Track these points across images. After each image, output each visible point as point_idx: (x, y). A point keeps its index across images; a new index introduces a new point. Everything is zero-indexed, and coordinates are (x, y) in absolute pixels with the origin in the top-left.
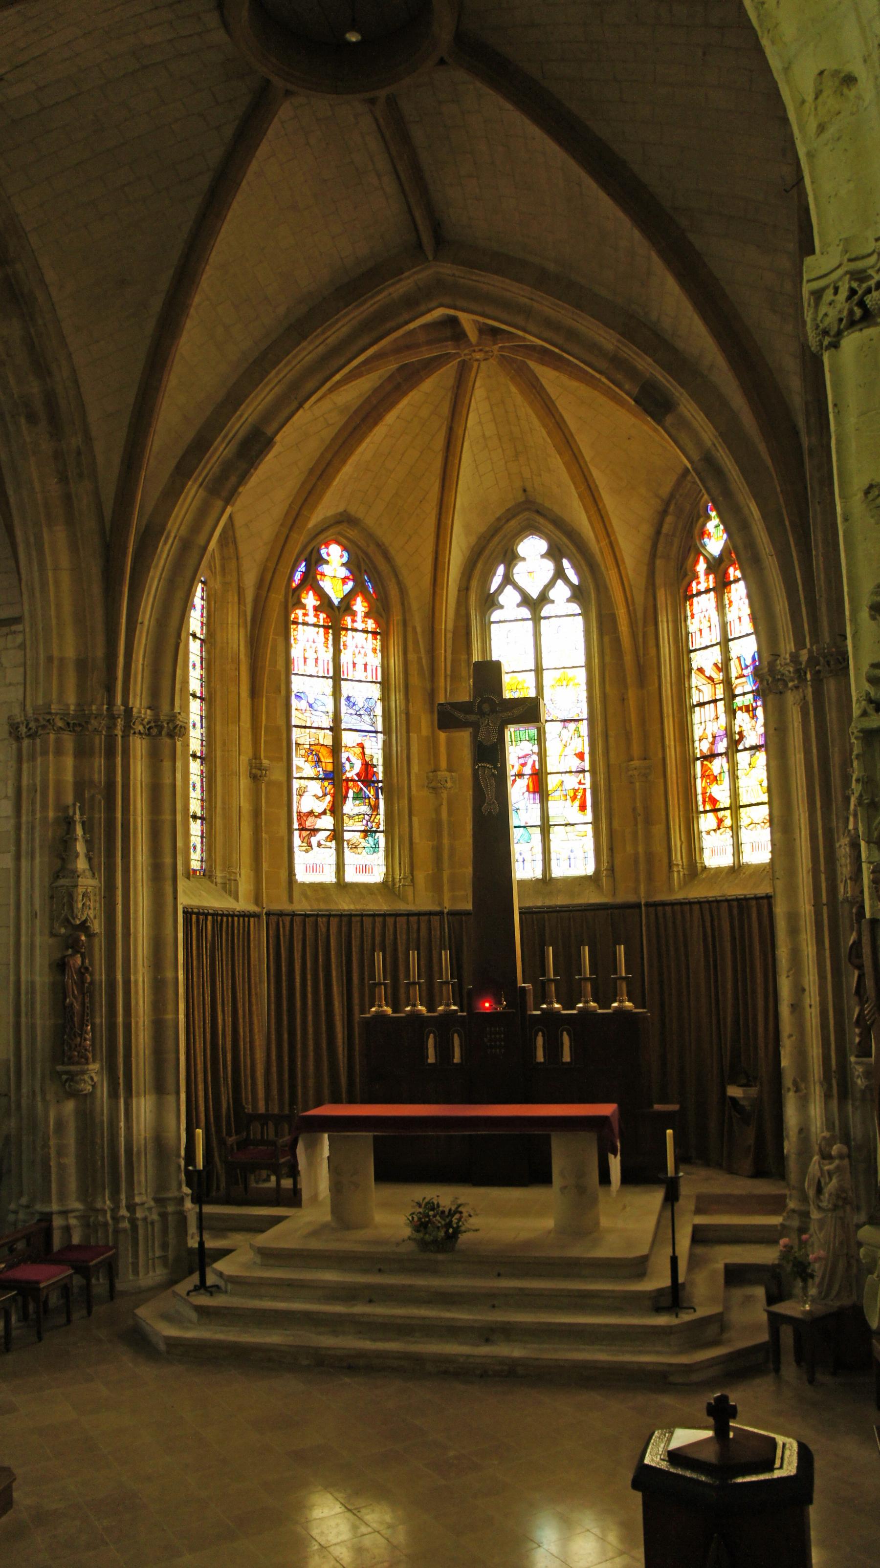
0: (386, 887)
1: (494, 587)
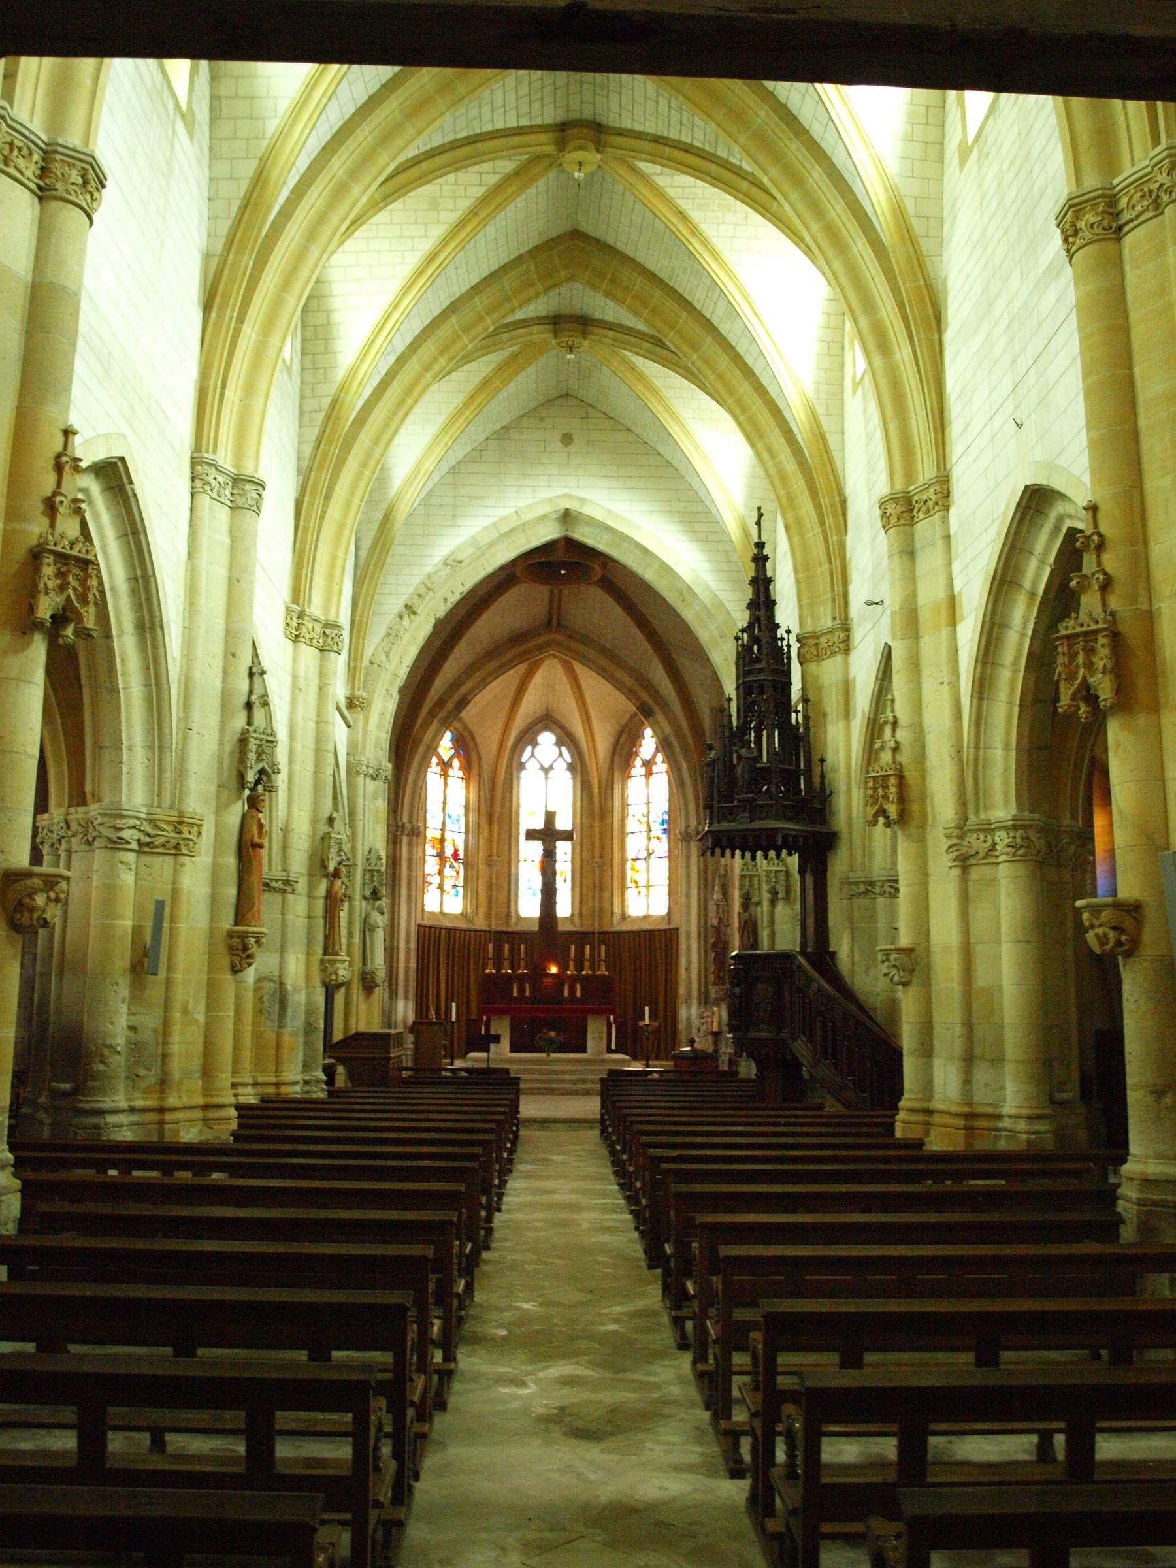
0: (464, 915)
1: (524, 759)
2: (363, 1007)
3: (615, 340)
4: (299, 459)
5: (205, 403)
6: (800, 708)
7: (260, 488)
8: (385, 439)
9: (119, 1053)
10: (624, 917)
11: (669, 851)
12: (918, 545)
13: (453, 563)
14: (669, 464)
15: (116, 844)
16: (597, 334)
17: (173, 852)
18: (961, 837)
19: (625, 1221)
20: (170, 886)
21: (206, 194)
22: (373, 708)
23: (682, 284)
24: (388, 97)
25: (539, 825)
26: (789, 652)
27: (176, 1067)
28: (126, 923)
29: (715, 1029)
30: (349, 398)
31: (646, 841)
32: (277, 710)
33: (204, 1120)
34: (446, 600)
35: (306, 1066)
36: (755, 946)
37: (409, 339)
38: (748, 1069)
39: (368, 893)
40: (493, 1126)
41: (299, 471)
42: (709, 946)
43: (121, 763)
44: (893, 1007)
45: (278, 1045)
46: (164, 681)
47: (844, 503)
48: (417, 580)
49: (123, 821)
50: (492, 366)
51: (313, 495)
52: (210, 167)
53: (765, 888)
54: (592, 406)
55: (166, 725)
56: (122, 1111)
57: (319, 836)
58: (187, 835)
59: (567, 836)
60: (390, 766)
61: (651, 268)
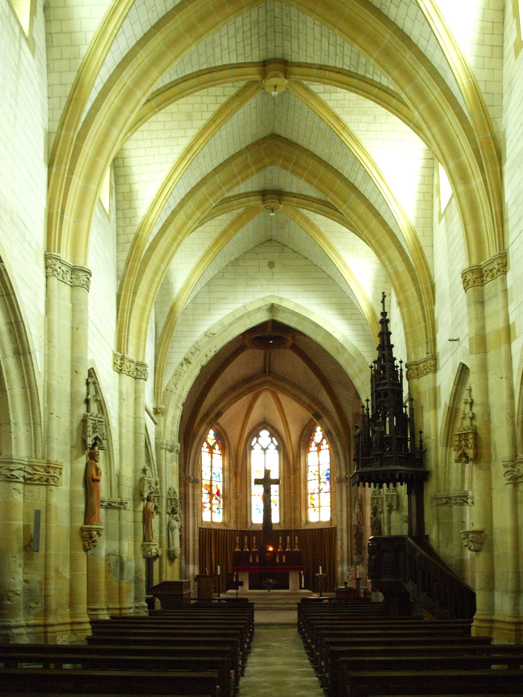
0: (223, 523)
1: (252, 444)
2: (169, 568)
3: (298, 203)
4: (117, 270)
5: (52, 222)
6: (407, 404)
7: (88, 275)
8: (167, 259)
9: (18, 595)
10: (307, 522)
11: (331, 489)
12: (486, 297)
13: (210, 335)
14: (329, 277)
15: (10, 479)
16: (287, 201)
17: (45, 483)
18: (513, 466)
19: (314, 682)
20: (45, 503)
21: (46, 94)
22: (168, 414)
23: (337, 163)
24: (156, 34)
25: (261, 476)
26: (401, 373)
27: (53, 602)
28: (19, 523)
29: (358, 577)
30: (145, 234)
31: (318, 484)
32: (111, 411)
33: (71, 630)
34: (206, 356)
35: (136, 599)
36: (380, 534)
37: (178, 200)
38: (380, 597)
39: (169, 511)
40: (237, 632)
41: (118, 277)
42: (353, 536)
43: (11, 432)
44: (462, 562)
45: (120, 589)
46: (34, 385)
47: (433, 287)
48: (190, 345)
49: (14, 465)
50: (228, 222)
51: (127, 291)
52: (48, 78)
53: (385, 504)
54: (285, 246)
55: (37, 411)
56: (22, 626)
57: (138, 479)
58: (53, 474)
59: (276, 482)
60: (179, 444)
61: (318, 154)
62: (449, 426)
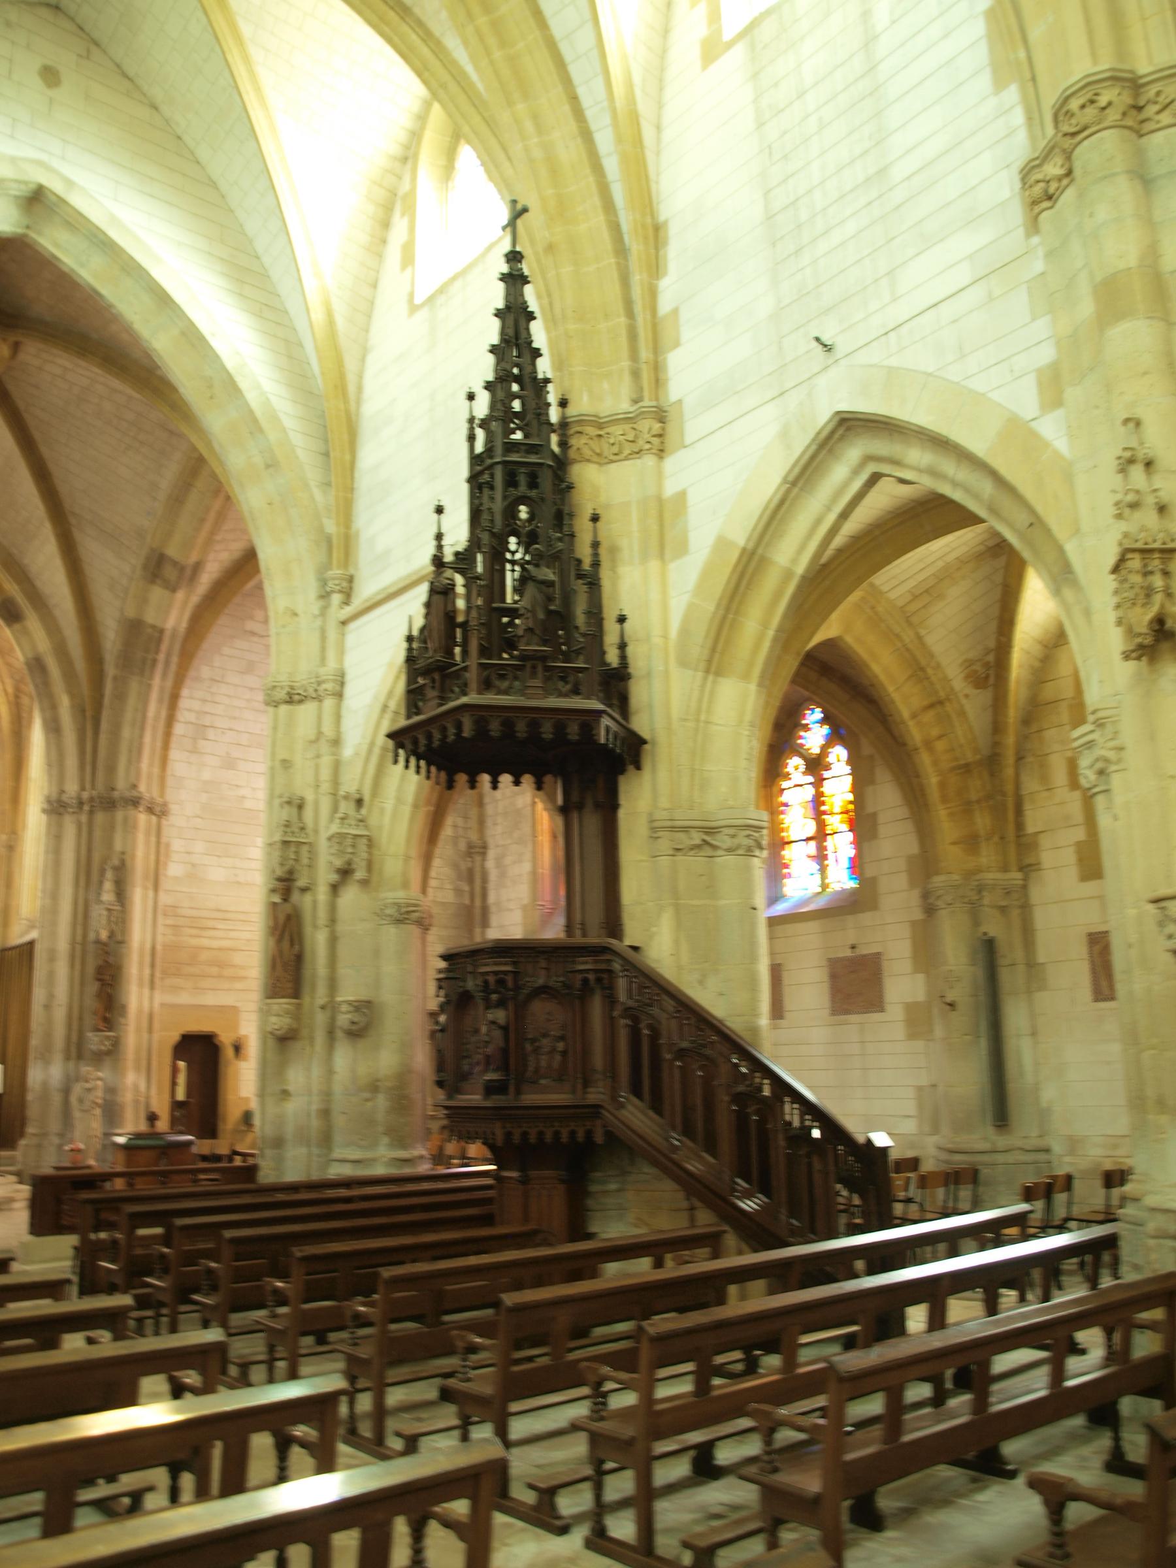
14: (214, 185)
62: (728, 609)
